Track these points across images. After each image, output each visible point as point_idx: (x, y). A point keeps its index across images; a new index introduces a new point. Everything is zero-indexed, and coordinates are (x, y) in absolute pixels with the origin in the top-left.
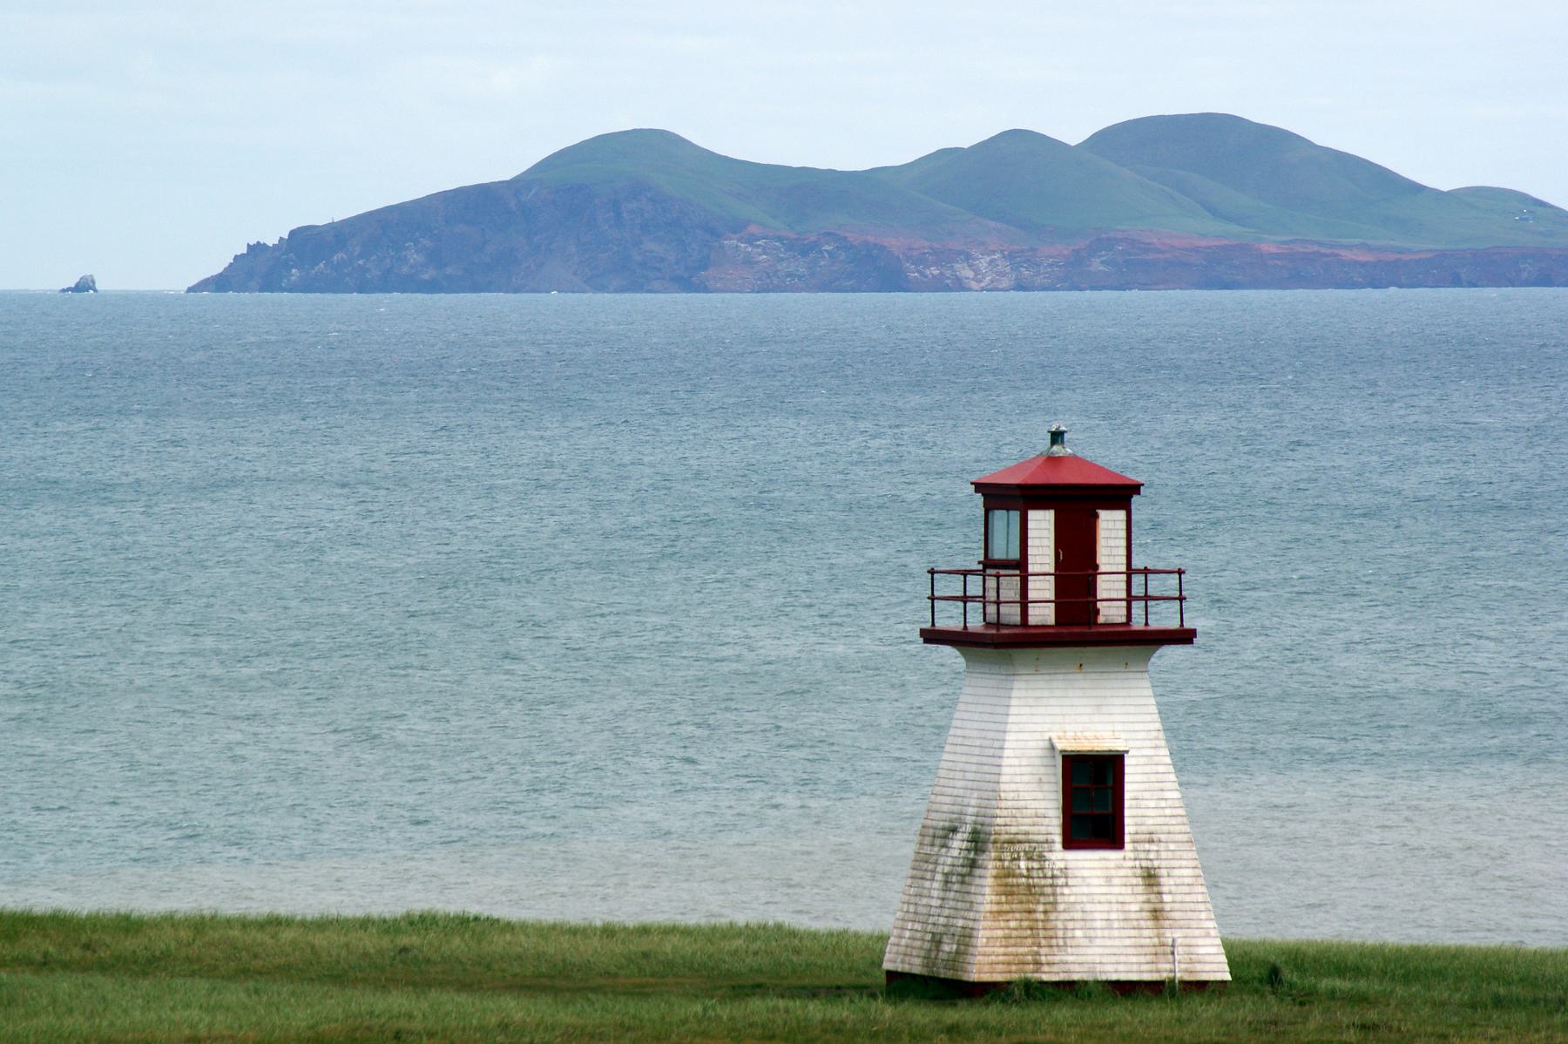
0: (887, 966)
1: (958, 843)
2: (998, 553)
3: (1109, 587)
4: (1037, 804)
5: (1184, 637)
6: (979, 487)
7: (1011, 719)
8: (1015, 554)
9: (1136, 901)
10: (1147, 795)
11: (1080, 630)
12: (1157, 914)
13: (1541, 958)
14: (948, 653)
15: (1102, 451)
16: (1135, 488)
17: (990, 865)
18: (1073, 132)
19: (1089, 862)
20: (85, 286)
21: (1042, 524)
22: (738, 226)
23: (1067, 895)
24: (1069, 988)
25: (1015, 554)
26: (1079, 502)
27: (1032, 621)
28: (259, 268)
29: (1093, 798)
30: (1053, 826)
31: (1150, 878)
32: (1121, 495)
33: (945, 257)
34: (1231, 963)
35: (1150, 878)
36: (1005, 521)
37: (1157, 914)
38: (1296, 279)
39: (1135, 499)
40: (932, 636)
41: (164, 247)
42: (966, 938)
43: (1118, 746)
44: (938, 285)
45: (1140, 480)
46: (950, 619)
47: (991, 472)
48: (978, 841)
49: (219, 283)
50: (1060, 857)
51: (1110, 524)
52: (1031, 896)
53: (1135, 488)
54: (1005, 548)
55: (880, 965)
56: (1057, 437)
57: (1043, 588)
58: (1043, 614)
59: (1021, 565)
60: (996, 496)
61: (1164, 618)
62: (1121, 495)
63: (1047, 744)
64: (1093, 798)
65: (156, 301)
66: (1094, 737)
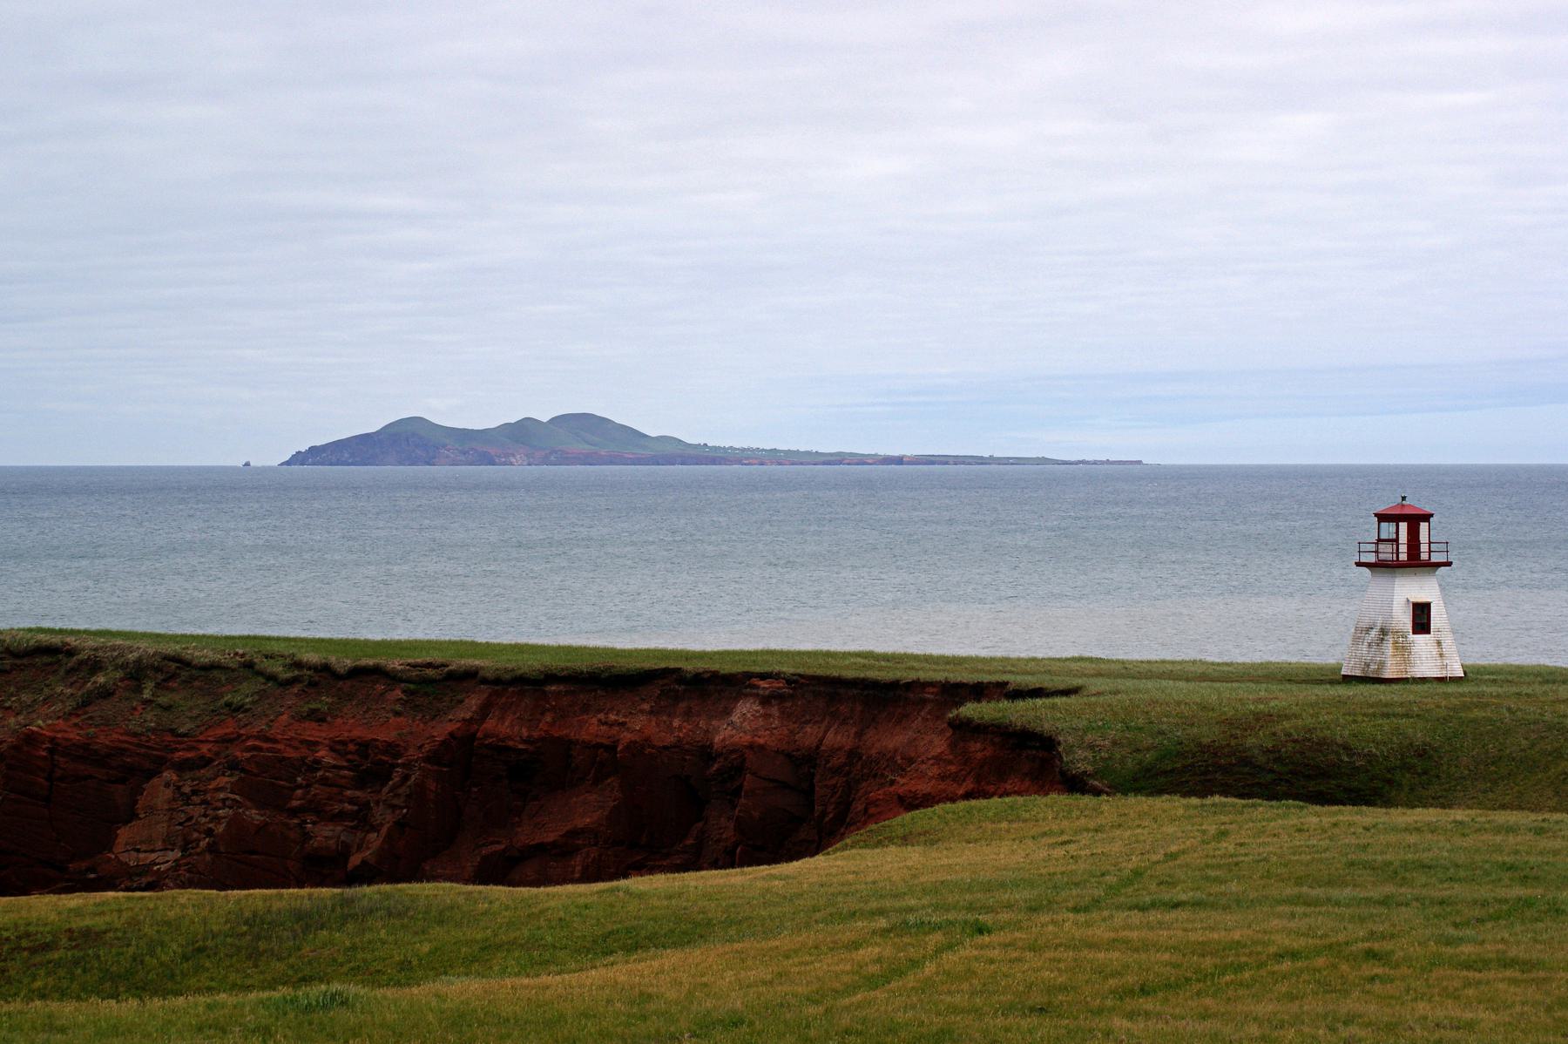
1: (1373, 633)
3: (1424, 548)
4: (1404, 620)
5: (1449, 564)
9: (1435, 651)
10: (1437, 617)
11: (1415, 562)
12: (1441, 655)
14: (1365, 570)
17: (1390, 639)
18: (545, 418)
19: (1421, 638)
20: (247, 464)
21: (1403, 526)
22: (444, 446)
23: (1415, 649)
24: (1424, 680)
26: (1415, 520)
28: (299, 459)
29: (1421, 617)
30: (1409, 627)
31: (1439, 643)
32: (1427, 517)
33: (507, 455)
35: (1439, 643)
37: (1441, 655)
38: (612, 463)
40: (1359, 564)
41: (271, 454)
42: (1382, 664)
44: (505, 464)
45: (1428, 509)
47: (1381, 508)
48: (1384, 632)
49: (288, 463)
50: (1412, 637)
51: (1424, 526)
52: (1403, 649)
56: (1404, 498)
57: (1403, 548)
58: (1403, 557)
59: (1397, 540)
60: (1382, 518)
62: (1427, 517)
64: (1421, 617)
65: (270, 468)
66: (1422, 598)
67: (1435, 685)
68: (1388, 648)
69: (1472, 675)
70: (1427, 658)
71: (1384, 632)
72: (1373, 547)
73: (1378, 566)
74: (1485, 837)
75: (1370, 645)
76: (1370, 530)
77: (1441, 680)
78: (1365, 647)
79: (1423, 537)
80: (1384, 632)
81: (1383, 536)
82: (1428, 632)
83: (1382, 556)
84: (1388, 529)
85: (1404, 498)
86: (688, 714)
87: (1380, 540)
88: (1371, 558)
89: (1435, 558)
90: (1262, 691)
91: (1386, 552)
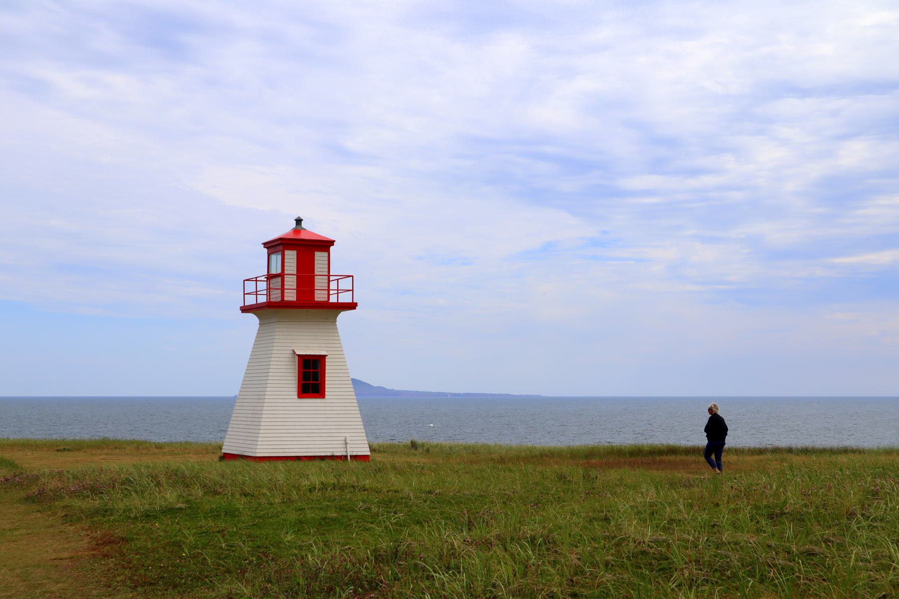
0: (223, 451)
2: (273, 272)
5: (352, 306)
6: (265, 244)
7: (259, 443)
8: (279, 271)
13: (486, 395)
15: (316, 228)
16: (332, 243)
21: (291, 256)
25: (279, 271)
27: (286, 299)
32: (325, 245)
34: (368, 422)
36: (276, 259)
39: (332, 248)
40: (245, 309)
43: (333, 239)
46: (251, 301)
51: (320, 257)
53: (332, 243)
54: (276, 269)
55: (221, 449)
57: (291, 282)
58: (291, 296)
61: (345, 298)
63: (291, 352)
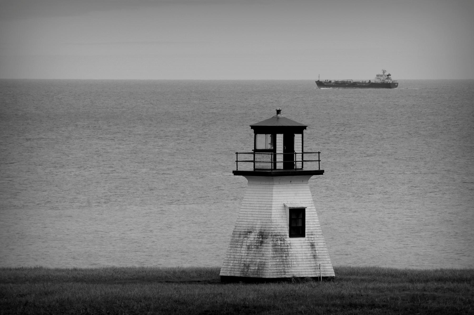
1: (253, 237)
3: (298, 158)
4: (282, 224)
5: (320, 172)
9: (309, 254)
10: (312, 222)
11: (291, 171)
12: (315, 257)
14: (241, 178)
19: (296, 241)
21: (280, 138)
23: (292, 251)
26: (290, 132)
29: (297, 221)
30: (288, 234)
31: (312, 245)
32: (300, 129)
35: (312, 245)
37: (315, 257)
40: (236, 173)
42: (262, 266)
45: (303, 123)
50: (289, 240)
51: (298, 137)
52: (281, 251)
56: (278, 112)
57: (280, 158)
58: (280, 166)
62: (300, 129)
64: (297, 221)
66: (298, 204)
67: (314, 284)
68: (268, 249)
69: (343, 276)
70: (304, 259)
71: (263, 235)
72: (251, 157)
73: (256, 174)
74: (406, 292)
75: (249, 248)
76: (245, 140)
77: (316, 279)
78: (244, 251)
79: (297, 148)
80: (263, 235)
81: (259, 147)
82: (303, 235)
83: (258, 165)
84: (264, 141)
85: (278, 112)
86: (154, 284)
87: (256, 151)
88: (249, 167)
89: (308, 167)
90: (209, 289)
91: (264, 162)
